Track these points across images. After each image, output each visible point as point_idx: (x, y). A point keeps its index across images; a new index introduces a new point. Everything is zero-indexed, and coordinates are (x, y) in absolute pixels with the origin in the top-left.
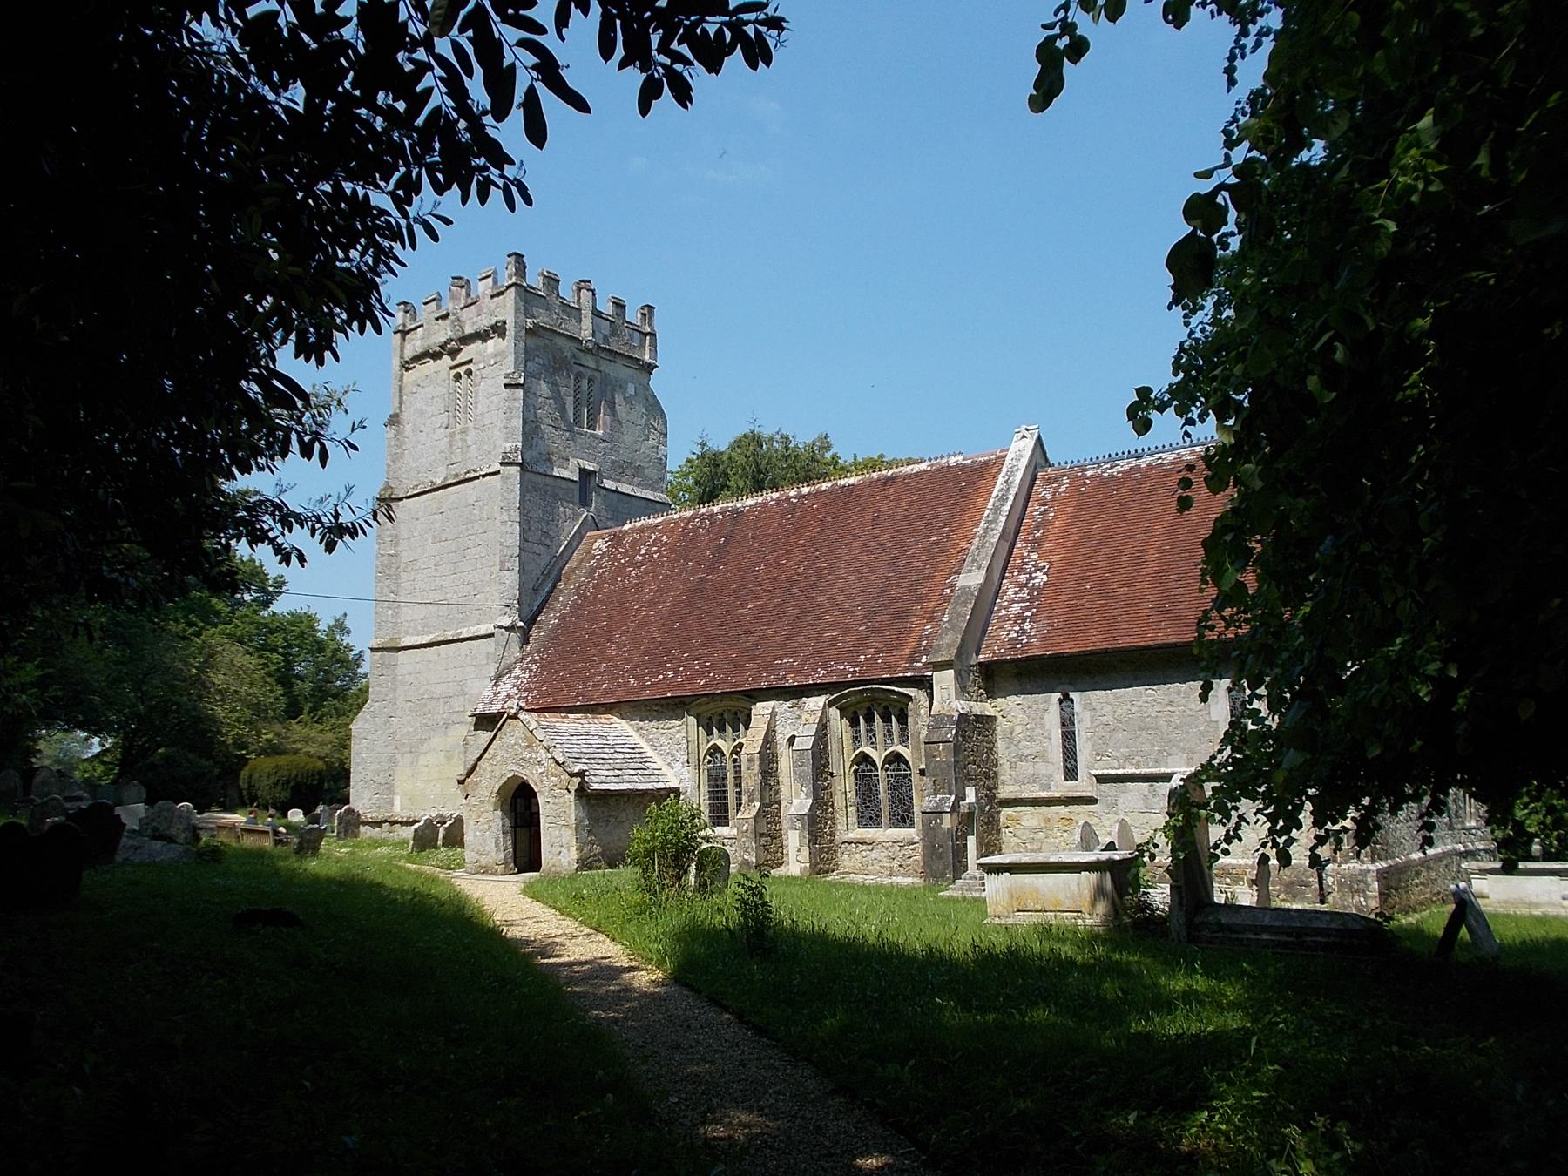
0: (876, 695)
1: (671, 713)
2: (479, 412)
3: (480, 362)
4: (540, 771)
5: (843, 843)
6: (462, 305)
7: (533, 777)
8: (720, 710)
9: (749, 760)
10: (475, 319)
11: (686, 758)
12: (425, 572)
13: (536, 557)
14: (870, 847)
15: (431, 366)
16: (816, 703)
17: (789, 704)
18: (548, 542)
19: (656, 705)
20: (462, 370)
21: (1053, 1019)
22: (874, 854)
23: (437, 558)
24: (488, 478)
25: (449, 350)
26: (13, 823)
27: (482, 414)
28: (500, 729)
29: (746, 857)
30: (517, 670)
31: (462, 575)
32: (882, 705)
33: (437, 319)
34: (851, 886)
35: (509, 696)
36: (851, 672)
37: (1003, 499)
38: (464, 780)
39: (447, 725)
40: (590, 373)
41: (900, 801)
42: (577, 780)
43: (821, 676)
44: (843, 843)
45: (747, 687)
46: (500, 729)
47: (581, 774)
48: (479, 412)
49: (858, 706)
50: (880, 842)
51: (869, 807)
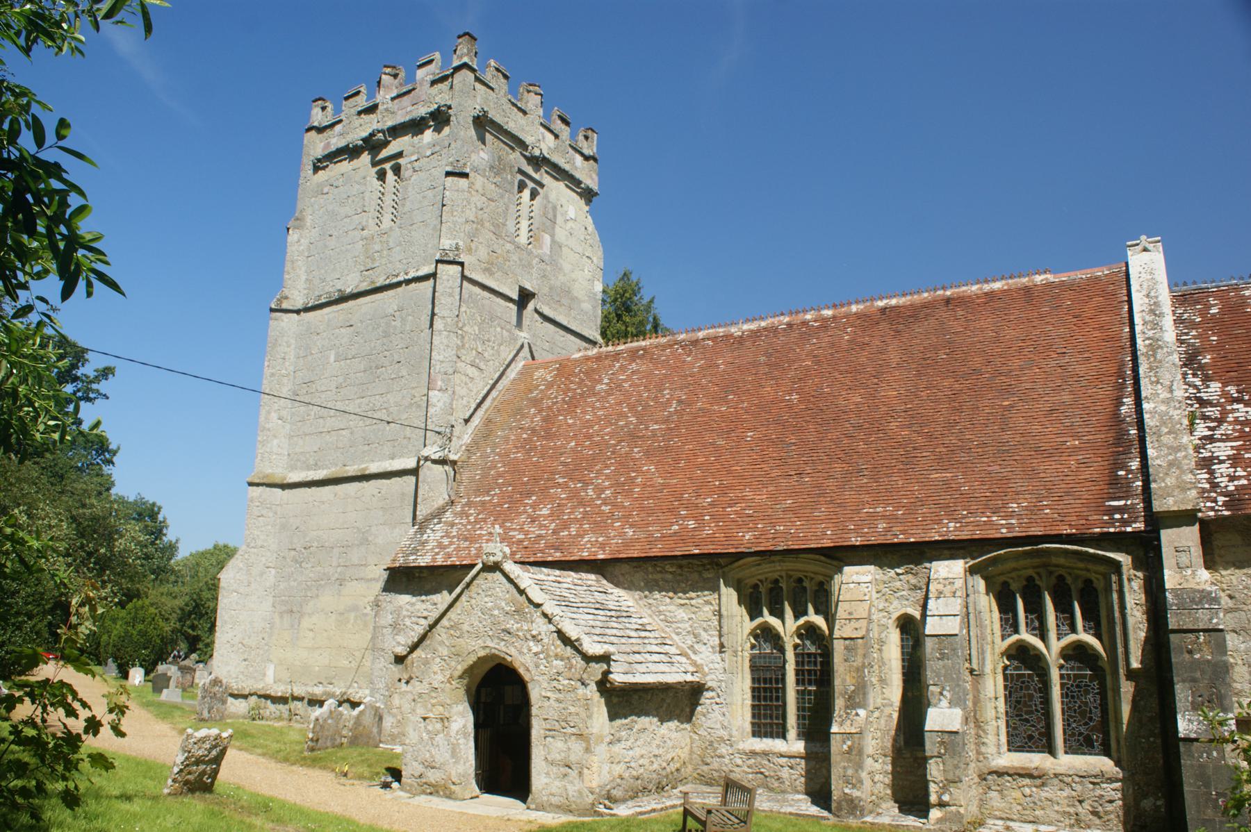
0: (1054, 560)
1: (695, 576)
2: (406, 209)
3: (412, 154)
4: (535, 649)
5: (990, 773)
6: (394, 95)
7: (523, 658)
8: (776, 576)
9: (846, 648)
10: (409, 109)
11: (717, 641)
12: (323, 396)
13: (468, 381)
14: (1038, 782)
15: (345, 166)
16: (950, 570)
17: (892, 573)
18: (482, 365)
19: (672, 565)
20: (387, 166)
21: (47, 783)
22: (1046, 793)
23: (341, 379)
24: (413, 285)
25: (372, 145)
26: (1070, 590)
27: (411, 211)
28: (468, 585)
29: (847, 791)
30: (448, 514)
31: (372, 399)
32: (1056, 574)
33: (360, 113)
34: (785, 813)
35: (441, 546)
36: (1003, 527)
37: (1154, 310)
38: (405, 657)
39: (341, 582)
40: (531, 185)
41: (1083, 714)
42: (598, 669)
43: (950, 530)
44: (990, 773)
45: (827, 543)
46: (468, 585)
47: (605, 658)
48: (406, 209)
49: (1014, 574)
50: (1056, 775)
51: (1027, 721)
